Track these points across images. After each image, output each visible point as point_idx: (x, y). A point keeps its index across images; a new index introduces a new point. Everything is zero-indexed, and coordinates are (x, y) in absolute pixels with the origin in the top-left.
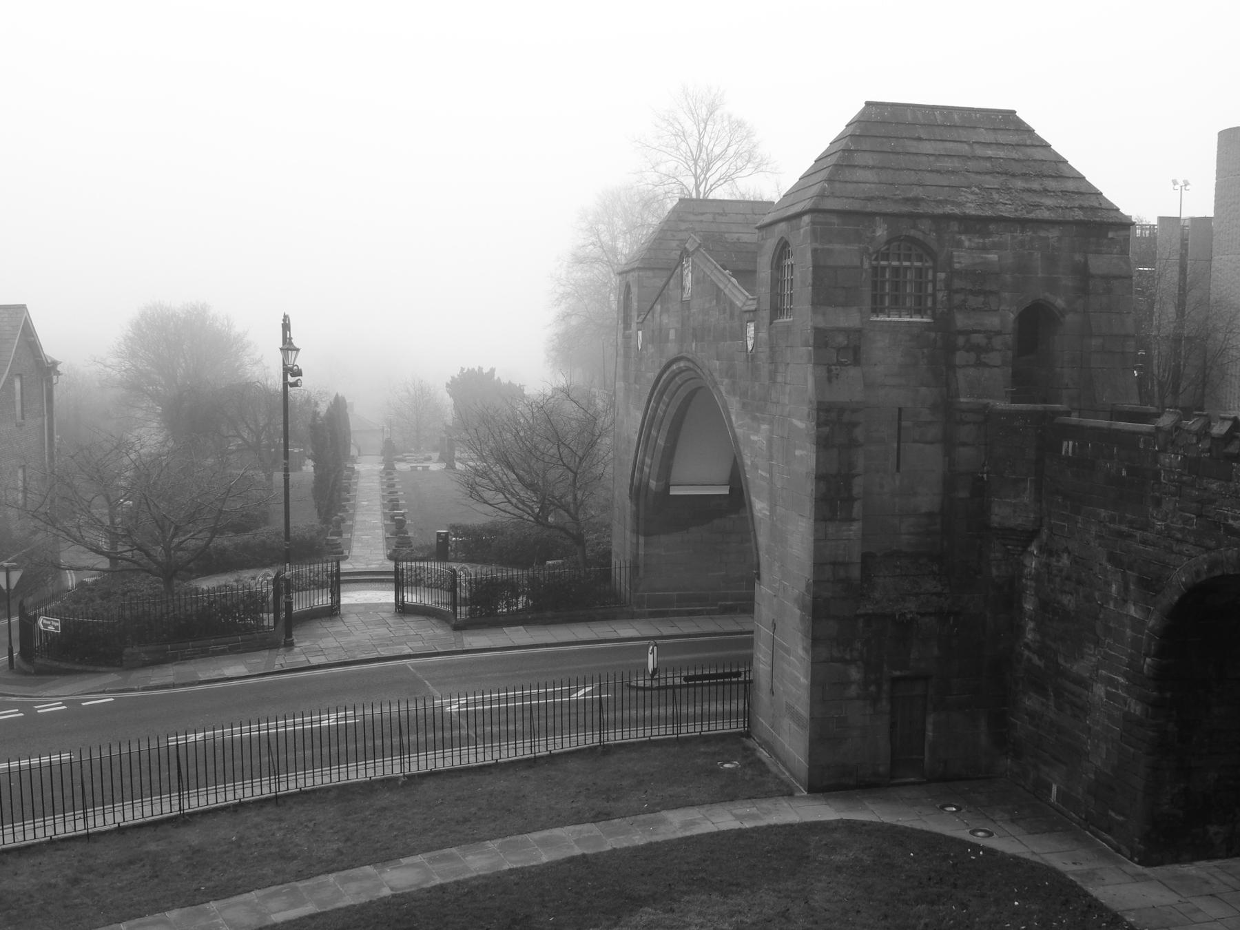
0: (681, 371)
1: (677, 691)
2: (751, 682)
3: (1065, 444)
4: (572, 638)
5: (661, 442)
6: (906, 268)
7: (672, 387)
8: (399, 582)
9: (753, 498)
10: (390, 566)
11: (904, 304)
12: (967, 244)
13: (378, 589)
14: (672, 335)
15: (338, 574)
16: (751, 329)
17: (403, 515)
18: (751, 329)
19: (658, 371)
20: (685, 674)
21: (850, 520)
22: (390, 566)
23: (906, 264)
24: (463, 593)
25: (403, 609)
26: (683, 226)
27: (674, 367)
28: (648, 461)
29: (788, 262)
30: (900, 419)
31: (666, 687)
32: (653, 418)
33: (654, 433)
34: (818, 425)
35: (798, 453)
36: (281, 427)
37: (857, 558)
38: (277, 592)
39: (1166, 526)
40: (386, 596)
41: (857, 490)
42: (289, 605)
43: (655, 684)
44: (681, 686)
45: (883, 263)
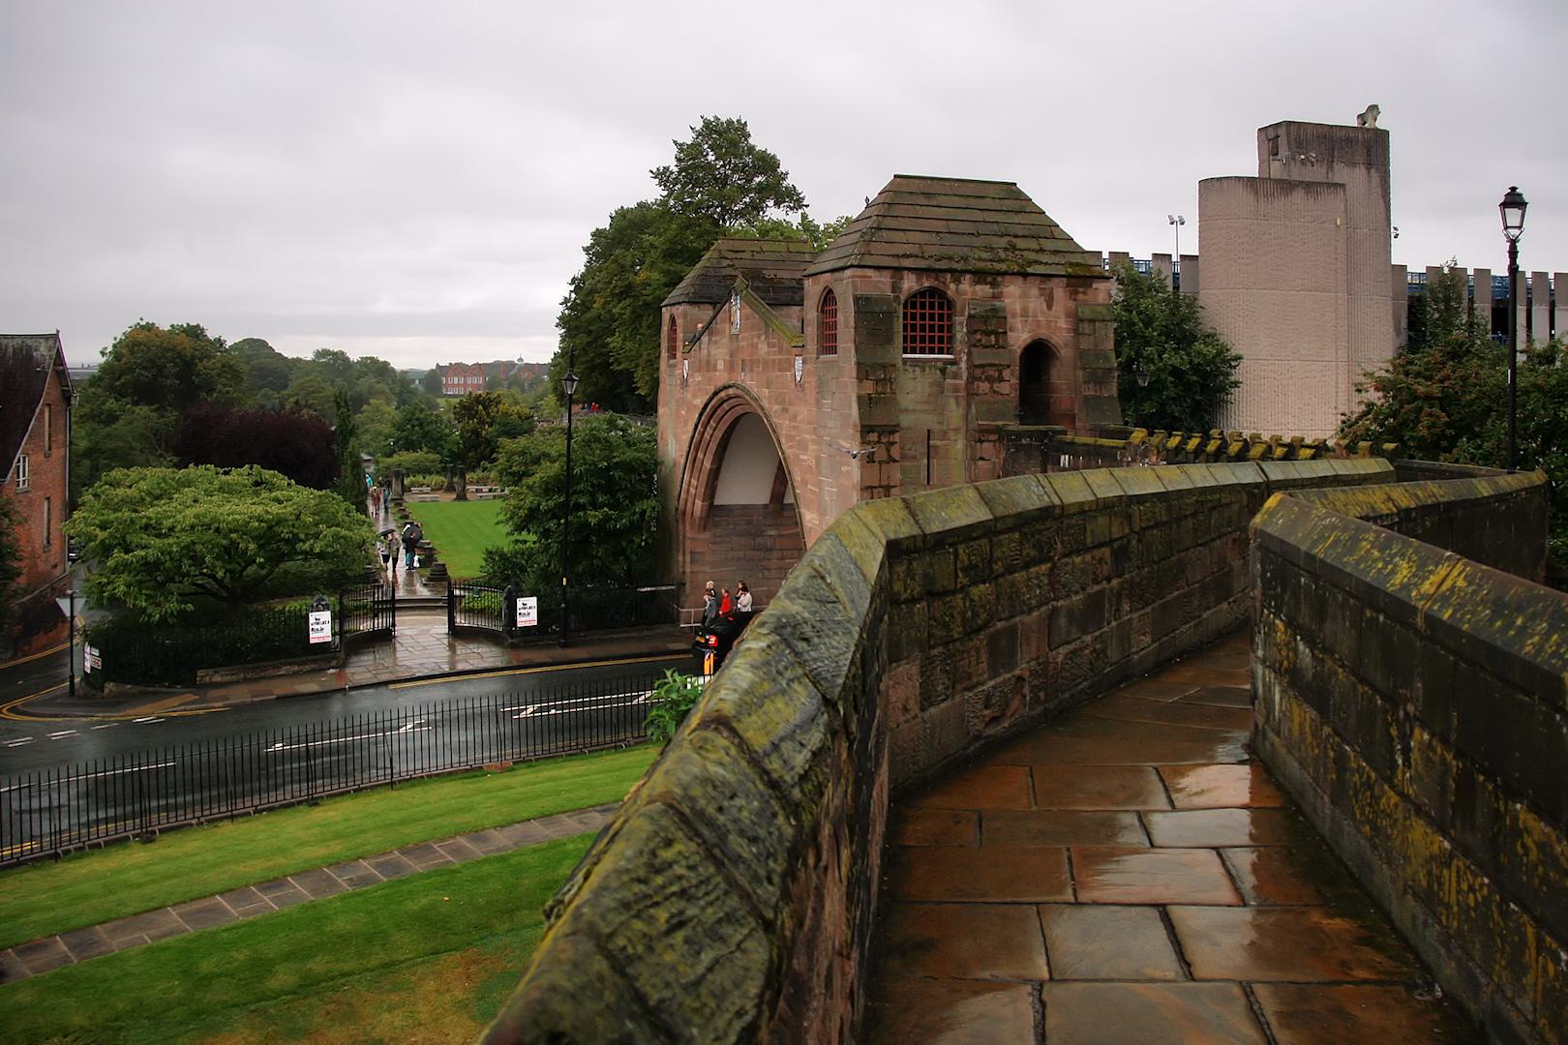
4: (626, 652)
5: (707, 465)
9: (803, 510)
14: (721, 365)
16: (799, 362)
18: (799, 362)
26: (726, 263)
27: (723, 394)
28: (694, 482)
33: (700, 455)
36: (865, 532)
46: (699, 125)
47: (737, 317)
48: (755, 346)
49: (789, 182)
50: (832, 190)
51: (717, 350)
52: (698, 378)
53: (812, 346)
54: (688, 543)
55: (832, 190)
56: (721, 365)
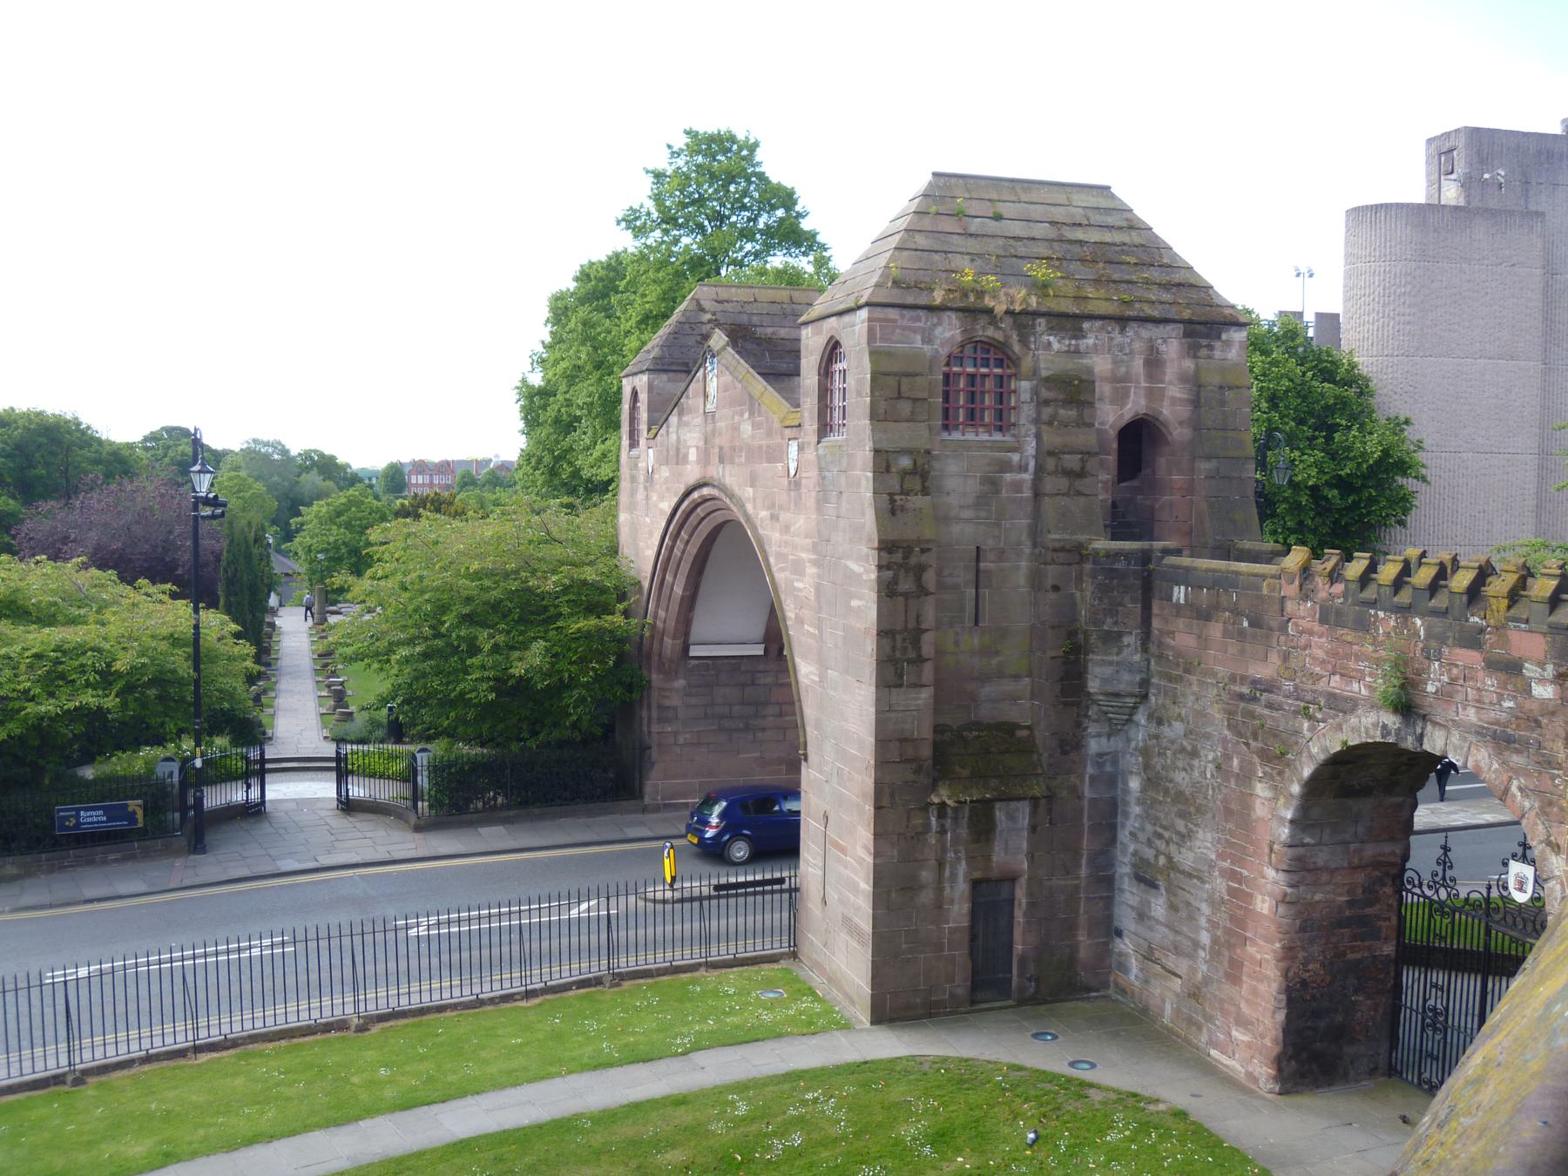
0: (705, 500)
1: (706, 903)
2: (796, 890)
3: (1176, 589)
5: (678, 590)
6: (984, 376)
7: (693, 519)
8: (342, 770)
9: (798, 660)
10: (329, 750)
11: (982, 418)
12: (1056, 346)
13: (312, 780)
14: (693, 455)
15: (263, 761)
17: (342, 684)
18: (793, 448)
19: (675, 500)
20: (714, 882)
21: (919, 686)
22: (329, 750)
23: (984, 370)
24: (423, 781)
25: (348, 806)
27: (695, 495)
28: (662, 614)
29: (838, 366)
30: (978, 560)
31: (692, 899)
32: (669, 559)
33: (669, 578)
34: (880, 567)
35: (855, 603)
37: (927, 733)
38: (184, 785)
39: (1296, 688)
40: (324, 789)
41: (927, 650)
42: (199, 801)
43: (677, 895)
44: (710, 898)
45: (955, 369)
46: (681, 141)
47: (712, 387)
48: (736, 428)
49: (805, 225)
50: (854, 218)
51: (687, 432)
52: (665, 472)
53: (811, 427)
54: (655, 694)
55: (854, 218)
56: (693, 455)
